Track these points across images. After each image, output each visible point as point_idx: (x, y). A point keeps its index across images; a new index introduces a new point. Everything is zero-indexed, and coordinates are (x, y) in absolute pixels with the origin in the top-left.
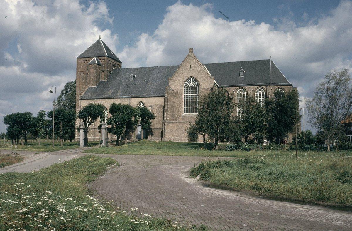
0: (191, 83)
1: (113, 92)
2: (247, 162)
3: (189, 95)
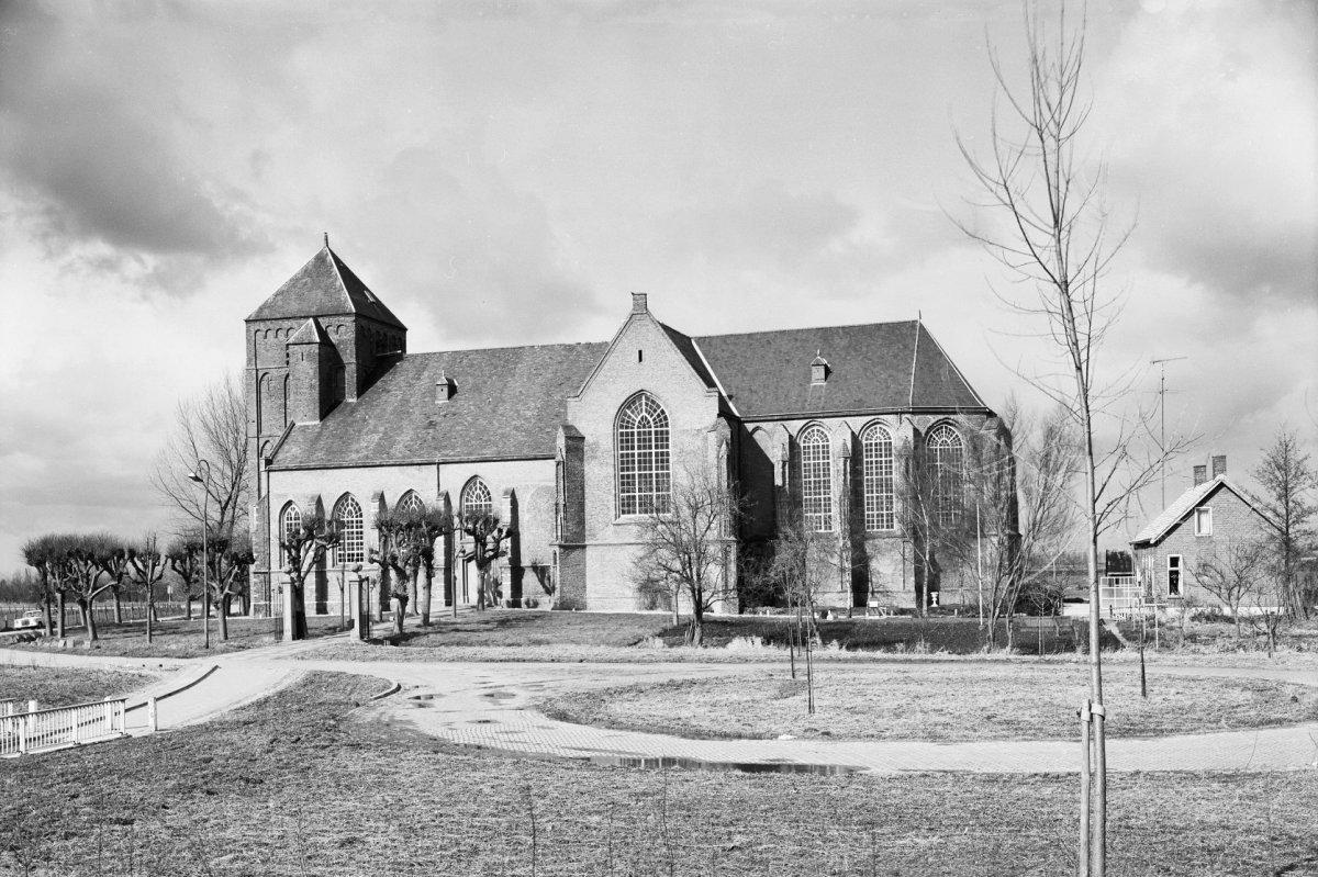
0: (644, 414)
1: (378, 444)
2: (1047, 463)
3: (654, 451)
